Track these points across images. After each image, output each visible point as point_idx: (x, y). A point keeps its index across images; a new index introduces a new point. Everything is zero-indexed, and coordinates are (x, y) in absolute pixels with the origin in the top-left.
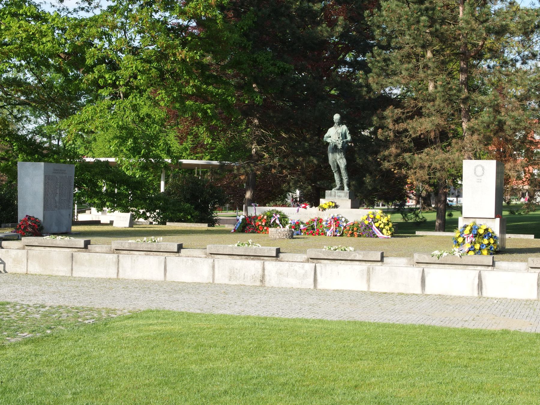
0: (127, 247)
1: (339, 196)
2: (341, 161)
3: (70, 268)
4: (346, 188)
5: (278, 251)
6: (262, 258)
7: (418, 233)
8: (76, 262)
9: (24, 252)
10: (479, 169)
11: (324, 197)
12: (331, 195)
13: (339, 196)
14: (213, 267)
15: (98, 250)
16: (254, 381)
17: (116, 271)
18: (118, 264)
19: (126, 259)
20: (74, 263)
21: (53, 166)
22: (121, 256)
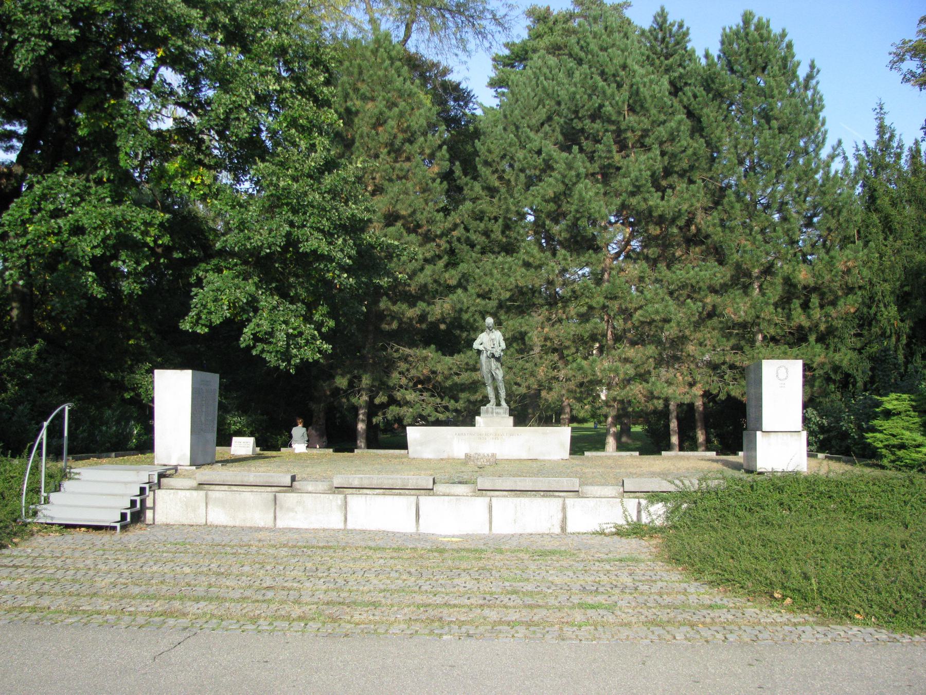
0: (356, 483)
1: (497, 413)
2: (497, 371)
3: (272, 515)
4: (503, 403)
5: (293, 479)
6: (557, 494)
7: (586, 453)
8: (281, 508)
9: (202, 493)
10: (783, 370)
11: (479, 414)
12: (487, 412)
13: (497, 413)
14: (490, 508)
15: (310, 488)
16: (362, 626)
17: (343, 518)
18: (346, 508)
19: (357, 502)
20: (278, 509)
21: (199, 373)
22: (349, 497)
